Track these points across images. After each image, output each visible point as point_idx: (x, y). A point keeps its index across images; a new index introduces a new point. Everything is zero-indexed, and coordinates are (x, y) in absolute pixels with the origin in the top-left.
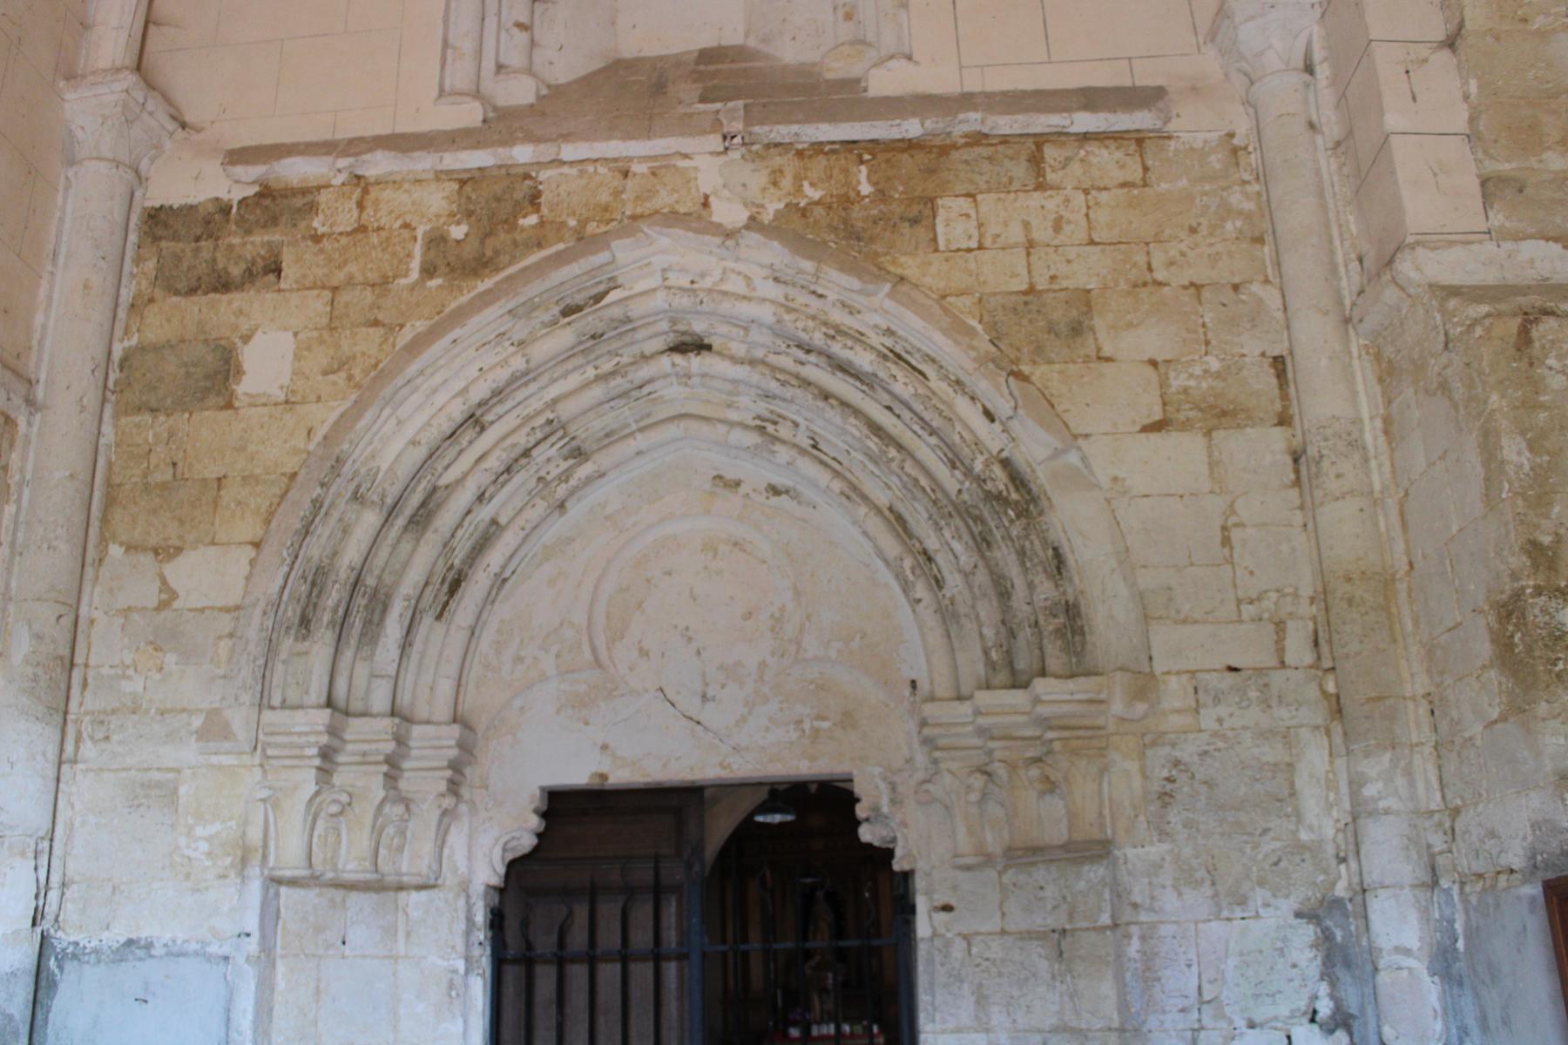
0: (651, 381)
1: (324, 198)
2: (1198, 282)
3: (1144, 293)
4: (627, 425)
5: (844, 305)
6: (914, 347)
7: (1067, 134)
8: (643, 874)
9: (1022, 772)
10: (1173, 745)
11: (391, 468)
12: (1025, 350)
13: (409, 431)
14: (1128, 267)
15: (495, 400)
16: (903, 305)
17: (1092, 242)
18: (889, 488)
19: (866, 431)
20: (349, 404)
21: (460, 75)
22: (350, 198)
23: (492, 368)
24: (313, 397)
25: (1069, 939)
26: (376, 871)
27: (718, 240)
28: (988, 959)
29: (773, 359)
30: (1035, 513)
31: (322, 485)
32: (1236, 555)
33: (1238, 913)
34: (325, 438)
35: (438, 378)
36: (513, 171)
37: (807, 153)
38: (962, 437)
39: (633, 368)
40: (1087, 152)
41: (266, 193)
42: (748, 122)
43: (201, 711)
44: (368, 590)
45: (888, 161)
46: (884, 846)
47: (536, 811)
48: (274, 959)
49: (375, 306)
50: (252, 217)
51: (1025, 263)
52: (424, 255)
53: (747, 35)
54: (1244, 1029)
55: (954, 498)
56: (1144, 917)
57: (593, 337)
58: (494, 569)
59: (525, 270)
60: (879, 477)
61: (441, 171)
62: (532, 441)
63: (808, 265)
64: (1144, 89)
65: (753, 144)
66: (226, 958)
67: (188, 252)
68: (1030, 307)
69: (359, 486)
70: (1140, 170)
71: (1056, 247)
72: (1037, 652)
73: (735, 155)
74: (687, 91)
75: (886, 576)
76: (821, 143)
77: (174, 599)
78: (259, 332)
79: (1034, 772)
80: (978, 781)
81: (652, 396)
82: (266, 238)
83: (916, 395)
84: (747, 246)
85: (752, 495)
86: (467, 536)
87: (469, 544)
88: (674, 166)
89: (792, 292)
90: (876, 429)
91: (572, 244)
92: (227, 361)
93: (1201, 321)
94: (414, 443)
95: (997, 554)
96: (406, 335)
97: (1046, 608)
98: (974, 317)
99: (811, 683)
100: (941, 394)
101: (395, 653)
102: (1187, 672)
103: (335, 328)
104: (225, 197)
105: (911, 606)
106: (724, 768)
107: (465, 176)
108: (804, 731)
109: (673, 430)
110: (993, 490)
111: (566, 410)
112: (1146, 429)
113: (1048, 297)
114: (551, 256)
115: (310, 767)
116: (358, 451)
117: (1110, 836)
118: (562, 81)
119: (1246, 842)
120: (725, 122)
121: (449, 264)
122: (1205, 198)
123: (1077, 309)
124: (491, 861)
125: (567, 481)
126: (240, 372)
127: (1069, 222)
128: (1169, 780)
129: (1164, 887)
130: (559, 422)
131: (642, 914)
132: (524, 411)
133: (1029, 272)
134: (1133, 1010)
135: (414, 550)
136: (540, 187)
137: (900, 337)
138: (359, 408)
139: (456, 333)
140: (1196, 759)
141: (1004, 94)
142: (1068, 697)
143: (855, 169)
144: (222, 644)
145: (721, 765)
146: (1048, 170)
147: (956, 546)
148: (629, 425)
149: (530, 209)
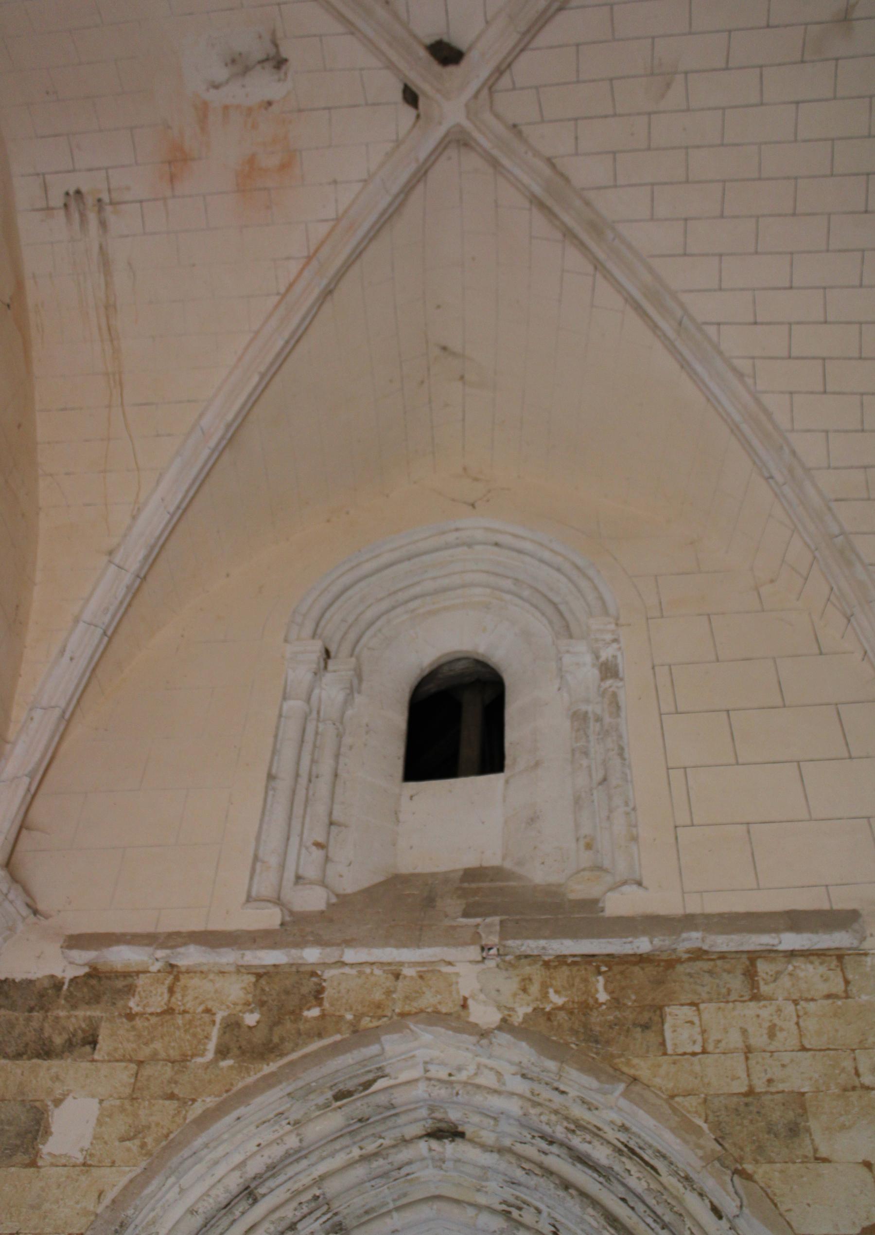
0: (410, 1163)
1: (141, 981)
3: (854, 1096)
4: (385, 1204)
5: (584, 1102)
6: (646, 1143)
7: (776, 951)
12: (748, 1149)
14: (837, 1072)
15: (269, 1174)
17: (803, 1049)
21: (265, 885)
22: (163, 983)
23: (269, 1144)
24: (107, 1162)
27: (473, 1039)
29: (519, 1148)
34: (114, 1201)
35: (220, 1151)
36: (302, 969)
37: (552, 964)
40: (795, 967)
41: (94, 973)
42: (503, 936)
45: (622, 973)
49: (173, 1081)
50: (79, 995)
51: (744, 1067)
52: (220, 1038)
53: (504, 858)
57: (360, 1120)
59: (305, 1056)
61: (242, 966)
62: (299, 1214)
63: (552, 1065)
64: (839, 911)
65: (506, 955)
67: (21, 1021)
68: (751, 1108)
71: (772, 1052)
73: (491, 964)
74: (452, 905)
76: (565, 956)
78: (69, 1099)
81: (409, 1177)
82: (88, 1013)
83: (649, 1189)
84: (499, 1045)
88: (439, 971)
89: (538, 1088)
91: (347, 1035)
92: (38, 1122)
94: (192, 1211)
96: (197, 1109)
98: (700, 1117)
100: (672, 1190)
103: (136, 1099)
104: (59, 974)
107: (261, 971)
109: (426, 1211)
111: (333, 1187)
113: (766, 1099)
116: (141, 1216)
118: (349, 891)
120: (483, 935)
121: (240, 1047)
123: (793, 1110)
126: (47, 1132)
127: (782, 1030)
130: (325, 1198)
133: (748, 1076)
136: (324, 984)
137: (634, 1133)
138: (148, 1175)
139: (241, 1111)
141: (721, 915)
143: (594, 979)
146: (761, 983)
148: (388, 1203)
149: (314, 1003)
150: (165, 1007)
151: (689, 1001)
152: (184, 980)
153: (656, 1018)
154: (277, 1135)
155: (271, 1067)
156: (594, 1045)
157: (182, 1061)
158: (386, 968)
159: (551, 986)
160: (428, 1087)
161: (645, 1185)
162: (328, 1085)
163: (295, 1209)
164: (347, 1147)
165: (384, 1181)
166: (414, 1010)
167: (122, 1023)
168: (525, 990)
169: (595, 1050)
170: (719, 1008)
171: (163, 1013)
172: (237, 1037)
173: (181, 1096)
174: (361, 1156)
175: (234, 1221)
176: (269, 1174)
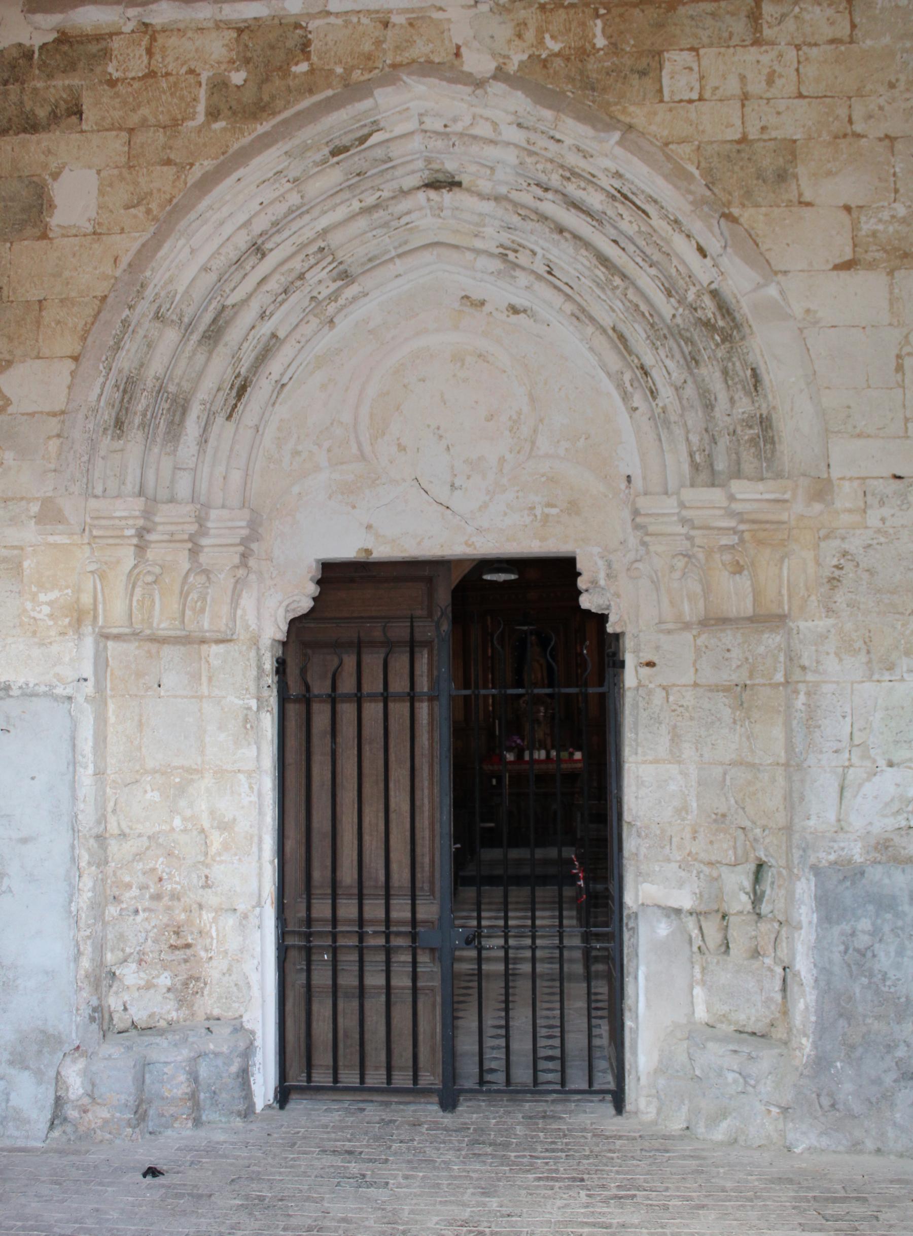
0: (408, 213)
1: (116, 44)
2: (893, 135)
3: (843, 144)
4: (387, 252)
6: (638, 189)
8: (400, 631)
9: (717, 556)
10: (843, 539)
11: (187, 292)
13: (202, 258)
14: (831, 119)
16: (632, 153)
17: (801, 96)
18: (614, 311)
19: (594, 261)
20: (149, 236)
22: (140, 45)
24: (117, 229)
25: (748, 692)
26: (184, 629)
27: (469, 89)
28: (682, 706)
29: (514, 195)
30: (737, 338)
31: (130, 307)
32: (906, 381)
33: (887, 676)
34: (130, 265)
35: (225, 211)
37: (548, 7)
38: (677, 270)
39: (393, 202)
40: (801, 9)
41: (64, 39)
43: (37, 499)
44: (170, 395)
45: (621, 15)
46: (600, 612)
47: (311, 579)
48: (106, 699)
50: (52, 62)
51: (739, 114)
52: (208, 99)
54: (885, 768)
55: (669, 321)
56: (810, 677)
57: (358, 175)
58: (275, 376)
59: (298, 114)
60: (605, 301)
61: (221, 21)
62: (306, 265)
63: (548, 114)
66: (70, 698)
68: (743, 155)
69: (160, 307)
70: (848, 27)
71: (768, 99)
72: (734, 456)
75: (609, 386)
77: (9, 405)
78: (66, 171)
79: (727, 557)
80: (680, 563)
82: (67, 82)
83: (640, 232)
85: (495, 313)
86: (251, 347)
87: (253, 355)
88: (430, 17)
89: (533, 137)
90: (604, 260)
91: (339, 90)
93: (892, 171)
94: (206, 269)
95: (704, 371)
96: (196, 173)
97: (743, 420)
98: (692, 164)
99: (543, 476)
101: (194, 449)
102: (858, 478)
103: (134, 167)
104: (27, 43)
105: (629, 413)
106: (469, 546)
107: (242, 25)
108: (536, 516)
110: (703, 318)
112: (836, 267)
114: (321, 102)
115: (130, 545)
117: (786, 612)
119: (898, 620)
121: (231, 108)
122: (905, 55)
123: (783, 157)
124: (276, 619)
125: (336, 301)
126: (52, 206)
127: (780, 76)
128: (839, 567)
129: (828, 654)
131: (400, 663)
132: (299, 239)
133: (743, 123)
134: (797, 750)
135: (208, 359)
136: (310, 36)
137: (627, 180)
140: (861, 551)
142: (759, 497)
144: (51, 442)
145: (466, 543)
146: (765, 26)
147: (668, 362)
148: (390, 251)
149: (302, 57)
150: (147, 71)
151: (689, 46)
152: (161, 39)
153: (654, 64)
154: (277, 193)
155: (262, 128)
156: (591, 92)
157: (173, 126)
158: (373, 16)
159: (547, 30)
160: (424, 138)
161: (637, 229)
162: (324, 141)
163: (303, 261)
164: (348, 200)
165: (385, 230)
166: (406, 61)
167: (104, 90)
168: (520, 36)
169: (591, 98)
170: (720, 53)
171: (145, 77)
172: (226, 97)
173: (178, 161)
174: (361, 208)
175: (246, 274)
176: (275, 229)
